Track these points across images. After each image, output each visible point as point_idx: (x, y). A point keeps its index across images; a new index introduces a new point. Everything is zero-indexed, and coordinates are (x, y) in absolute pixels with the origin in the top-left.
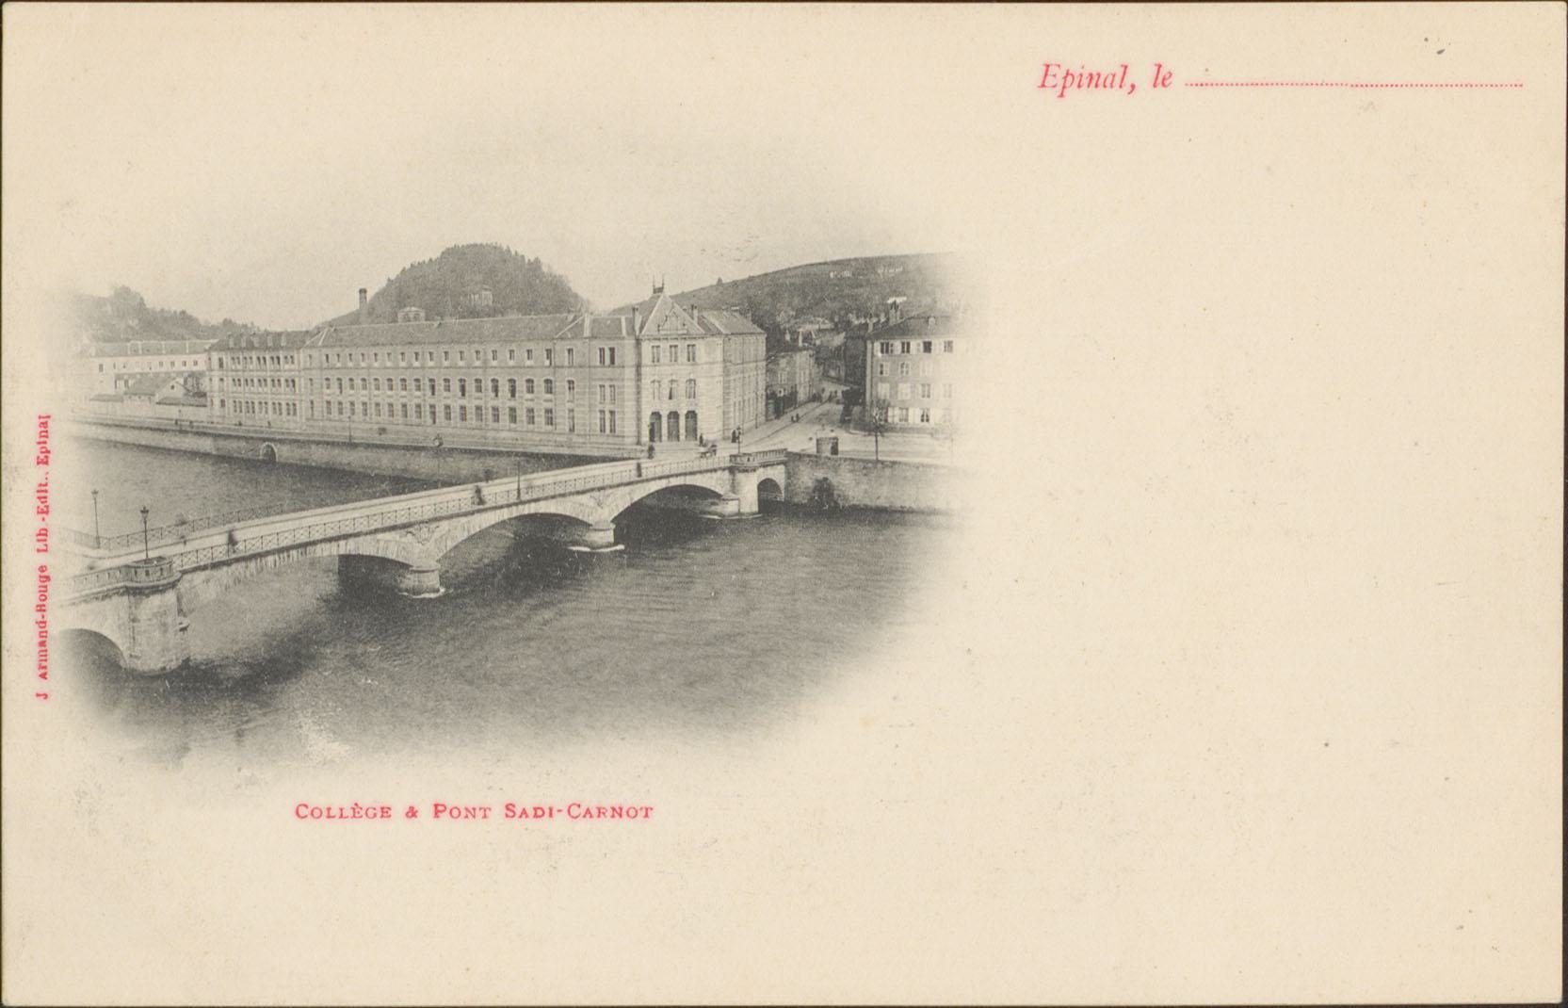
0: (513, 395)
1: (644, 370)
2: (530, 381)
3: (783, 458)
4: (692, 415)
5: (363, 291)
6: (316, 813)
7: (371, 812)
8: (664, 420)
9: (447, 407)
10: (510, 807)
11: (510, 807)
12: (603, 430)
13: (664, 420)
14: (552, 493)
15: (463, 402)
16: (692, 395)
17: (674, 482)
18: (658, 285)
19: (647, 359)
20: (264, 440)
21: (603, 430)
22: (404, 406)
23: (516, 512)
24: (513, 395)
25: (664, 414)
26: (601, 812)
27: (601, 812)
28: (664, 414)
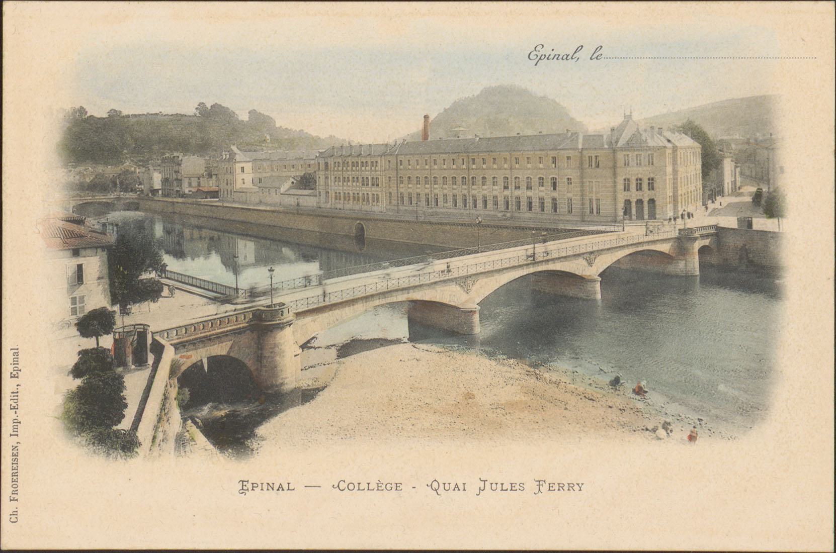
0: (555, 189)
1: (618, 170)
2: (541, 178)
3: (713, 231)
4: (652, 201)
5: (426, 117)
6: (351, 486)
7: (389, 487)
8: (633, 204)
9: (455, 196)
10: (539, 483)
11: (539, 483)
12: (591, 212)
13: (633, 204)
14: (564, 254)
15: (529, 193)
16: (651, 187)
17: (640, 249)
18: (628, 113)
19: (621, 163)
20: (358, 219)
21: (591, 212)
22: (418, 194)
23: (532, 270)
24: (555, 189)
25: (634, 200)
26: (561, 487)
27: (561, 487)
28: (634, 200)
